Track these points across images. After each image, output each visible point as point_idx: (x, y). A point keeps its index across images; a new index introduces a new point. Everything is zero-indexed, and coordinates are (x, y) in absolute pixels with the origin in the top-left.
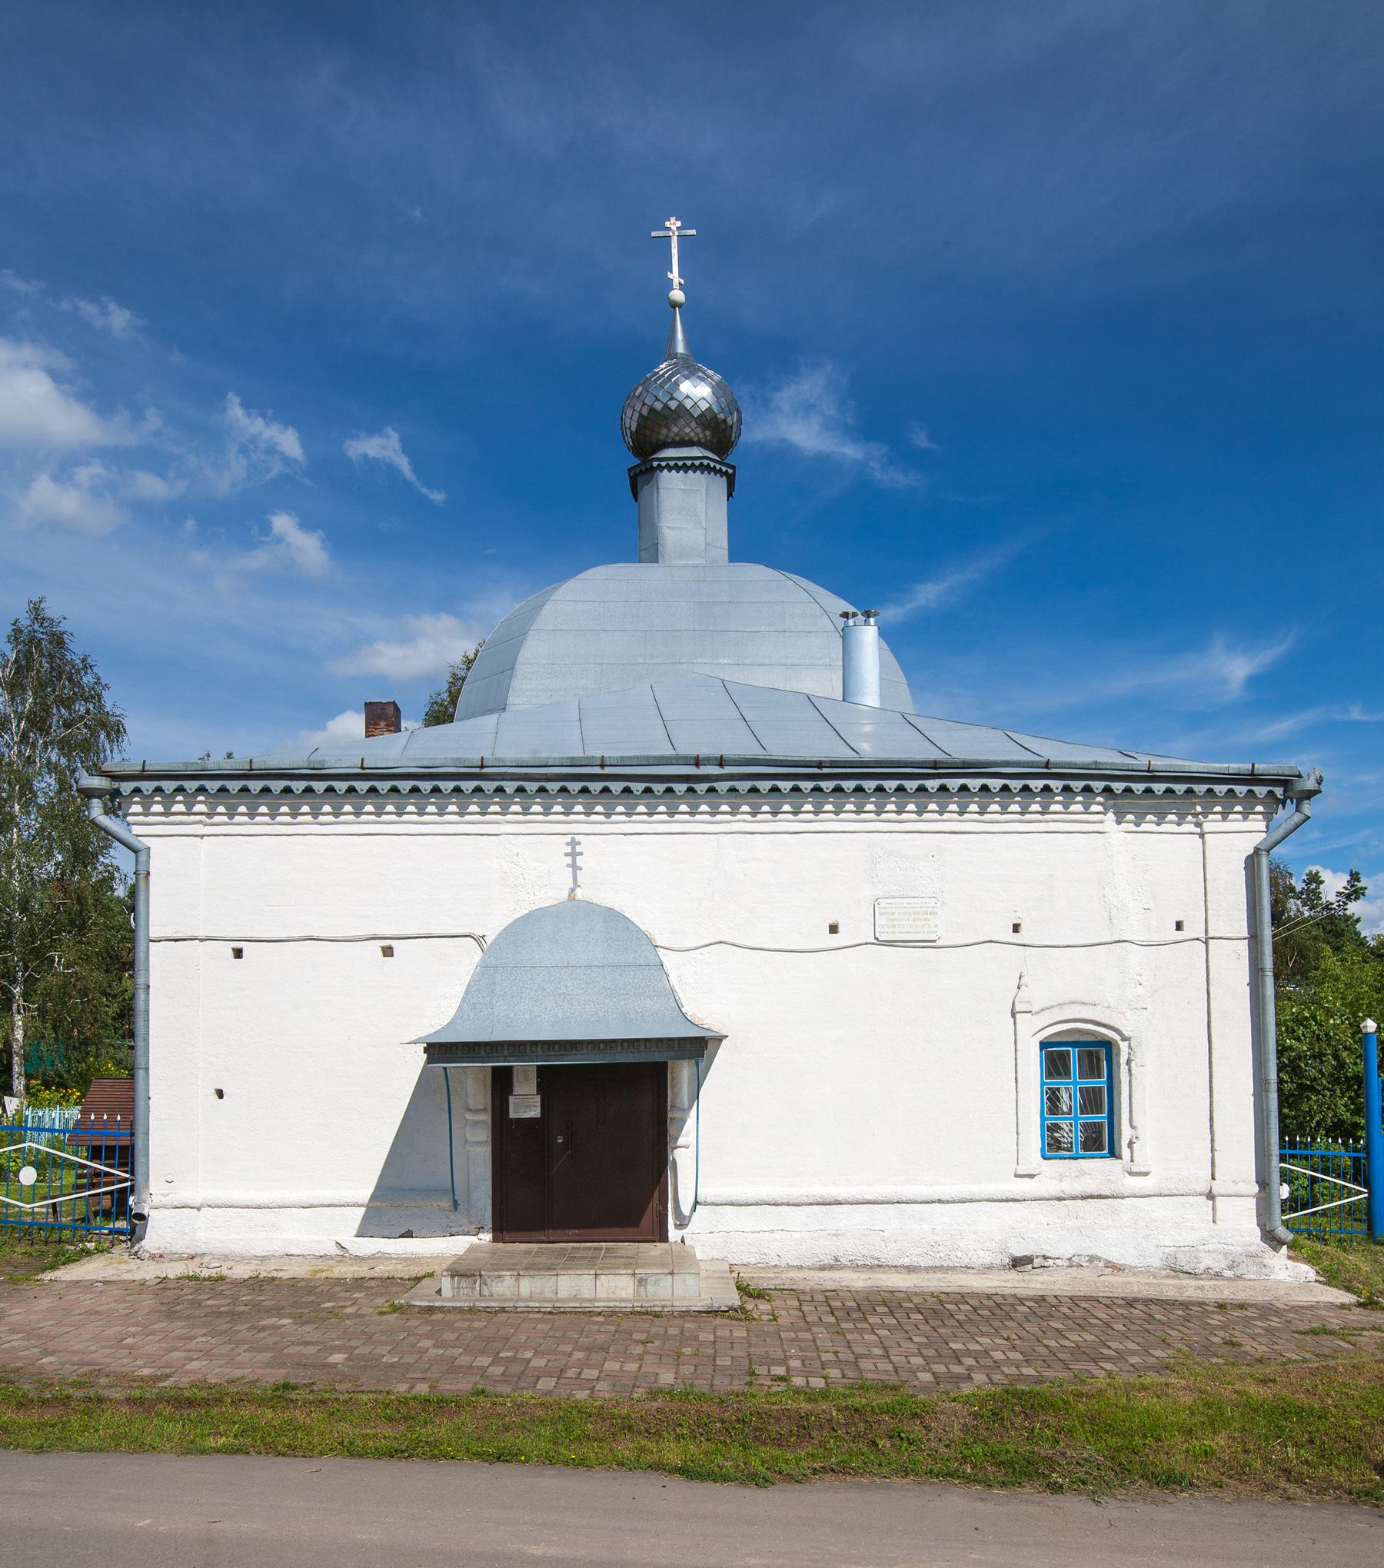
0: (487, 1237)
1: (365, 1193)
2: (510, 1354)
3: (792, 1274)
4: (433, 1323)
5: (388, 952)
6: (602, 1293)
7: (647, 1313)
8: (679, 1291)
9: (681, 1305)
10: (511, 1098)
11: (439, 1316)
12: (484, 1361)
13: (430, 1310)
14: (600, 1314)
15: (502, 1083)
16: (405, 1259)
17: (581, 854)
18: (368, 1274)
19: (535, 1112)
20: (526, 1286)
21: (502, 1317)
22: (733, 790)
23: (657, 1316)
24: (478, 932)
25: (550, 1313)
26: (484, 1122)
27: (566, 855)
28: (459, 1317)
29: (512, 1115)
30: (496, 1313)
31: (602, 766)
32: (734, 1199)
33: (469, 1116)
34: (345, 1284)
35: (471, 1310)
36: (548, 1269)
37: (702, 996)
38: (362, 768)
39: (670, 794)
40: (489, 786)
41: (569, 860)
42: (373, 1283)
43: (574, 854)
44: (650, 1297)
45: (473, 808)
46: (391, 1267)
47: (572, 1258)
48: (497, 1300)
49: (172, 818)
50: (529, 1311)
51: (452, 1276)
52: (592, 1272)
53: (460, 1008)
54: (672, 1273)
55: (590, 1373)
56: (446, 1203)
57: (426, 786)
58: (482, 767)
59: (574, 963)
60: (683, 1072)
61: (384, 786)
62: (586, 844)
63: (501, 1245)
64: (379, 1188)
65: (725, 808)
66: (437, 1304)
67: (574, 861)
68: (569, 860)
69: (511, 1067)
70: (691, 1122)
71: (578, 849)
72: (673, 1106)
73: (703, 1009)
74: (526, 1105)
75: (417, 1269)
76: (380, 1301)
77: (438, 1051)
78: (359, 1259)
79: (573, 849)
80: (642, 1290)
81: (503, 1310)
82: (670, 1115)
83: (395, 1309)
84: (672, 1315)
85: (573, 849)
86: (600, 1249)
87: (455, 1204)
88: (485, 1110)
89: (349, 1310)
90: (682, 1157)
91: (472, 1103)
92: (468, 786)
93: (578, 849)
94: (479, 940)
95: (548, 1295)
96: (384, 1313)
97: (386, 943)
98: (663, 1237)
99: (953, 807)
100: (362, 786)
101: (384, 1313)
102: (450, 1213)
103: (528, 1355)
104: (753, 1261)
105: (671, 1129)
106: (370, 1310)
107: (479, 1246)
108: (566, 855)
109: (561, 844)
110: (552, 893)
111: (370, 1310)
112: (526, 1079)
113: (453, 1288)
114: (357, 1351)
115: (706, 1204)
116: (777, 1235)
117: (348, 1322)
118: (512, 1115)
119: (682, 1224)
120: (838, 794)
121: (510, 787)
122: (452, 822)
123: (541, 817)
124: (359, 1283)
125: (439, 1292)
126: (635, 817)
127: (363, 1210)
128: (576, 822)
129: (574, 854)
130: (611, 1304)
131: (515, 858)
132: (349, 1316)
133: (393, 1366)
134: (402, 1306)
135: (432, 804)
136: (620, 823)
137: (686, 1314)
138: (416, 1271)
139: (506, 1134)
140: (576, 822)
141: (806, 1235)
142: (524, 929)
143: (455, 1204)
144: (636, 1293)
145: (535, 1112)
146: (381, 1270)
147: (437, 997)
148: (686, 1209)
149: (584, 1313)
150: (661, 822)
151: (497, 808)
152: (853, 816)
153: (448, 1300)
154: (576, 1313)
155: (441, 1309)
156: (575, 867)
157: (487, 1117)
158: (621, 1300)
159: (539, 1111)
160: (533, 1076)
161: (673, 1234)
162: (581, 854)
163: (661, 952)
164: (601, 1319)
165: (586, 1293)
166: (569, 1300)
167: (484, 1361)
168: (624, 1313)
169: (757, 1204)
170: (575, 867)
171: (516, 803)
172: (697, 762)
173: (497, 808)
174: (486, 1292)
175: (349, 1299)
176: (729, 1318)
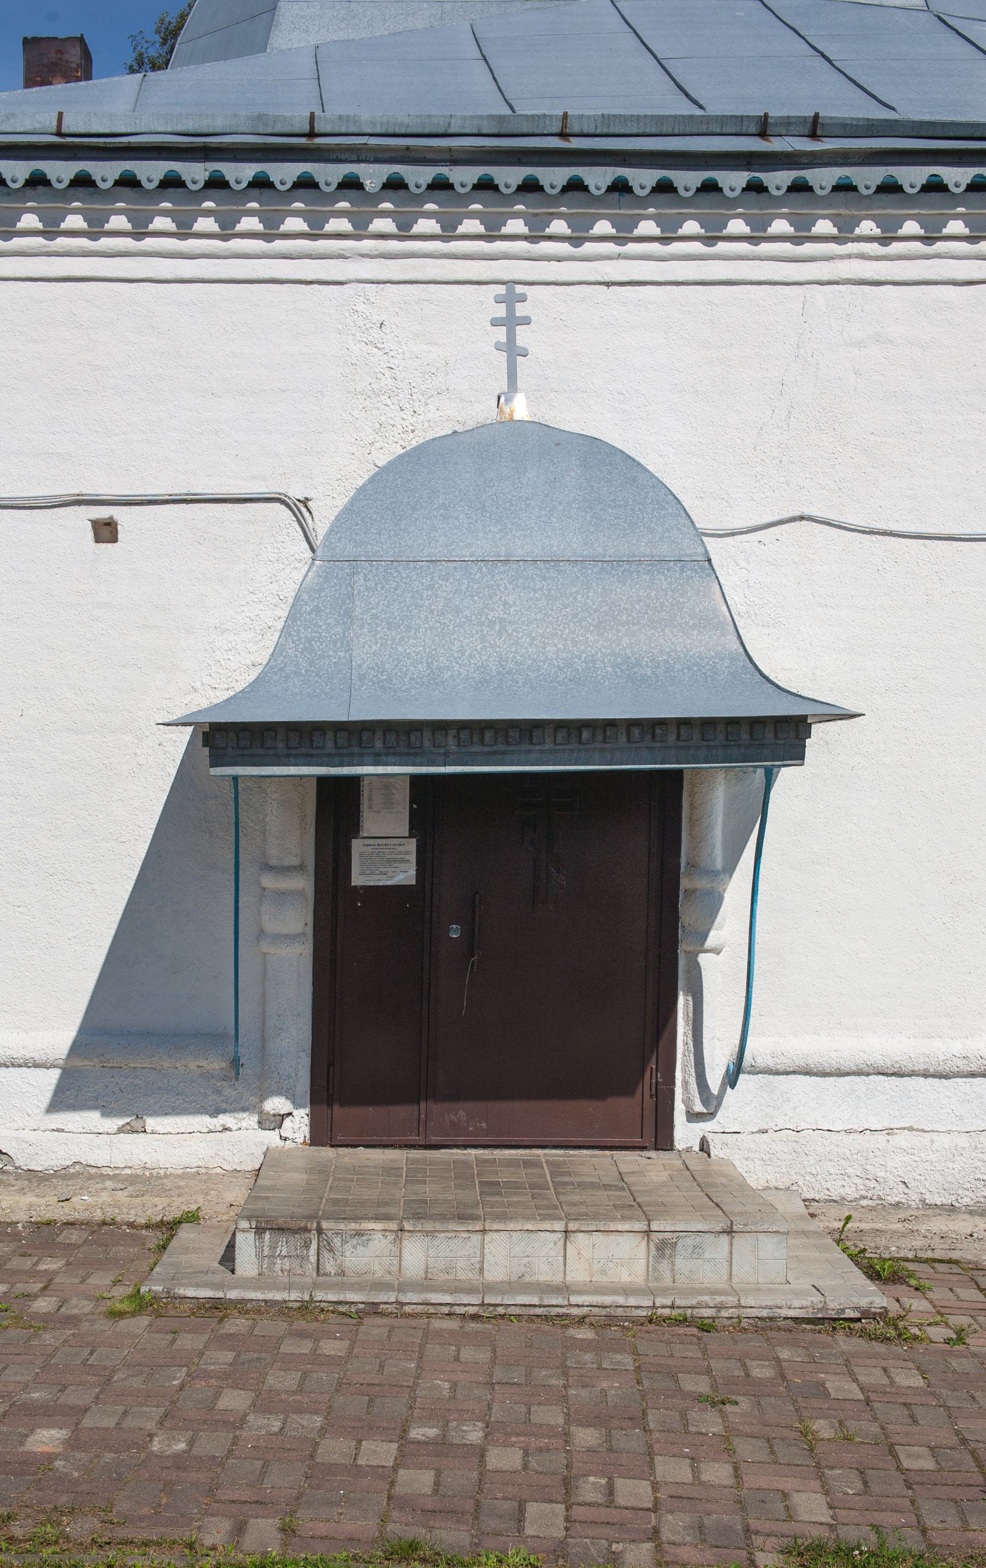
0: (299, 1125)
1: (59, 1038)
2: (433, 1432)
3: (939, 1224)
4: (227, 1341)
5: (106, 531)
6: (577, 1274)
7: (683, 1321)
8: (744, 1271)
9: (756, 1305)
10: (356, 844)
11: (236, 1325)
12: (379, 1452)
13: (218, 1308)
14: (581, 1320)
15: (338, 808)
16: (133, 1179)
17: (526, 321)
18: (61, 1213)
19: (404, 874)
20: (417, 1255)
21: (374, 1328)
22: (844, 187)
23: (706, 1327)
24: (296, 493)
25: (475, 1317)
26: (300, 893)
27: (495, 323)
28: (283, 1325)
29: (358, 879)
30: (361, 1315)
31: (563, 135)
32: (813, 1061)
33: (268, 881)
34: (16, 1236)
35: (305, 1308)
36: (462, 1218)
37: (788, 626)
38: (59, 134)
39: (713, 196)
40: (329, 174)
41: (501, 334)
42: (74, 1236)
43: (511, 322)
44: (682, 1282)
45: (294, 224)
46: (105, 1197)
47: (491, 1187)
48: (357, 1287)
49: (280, 245)
50: (430, 1312)
51: (259, 1231)
52: (559, 1226)
53: (279, 650)
54: (730, 1232)
55: (635, 1492)
56: (216, 1064)
57: (195, 172)
58: (312, 134)
59: (520, 553)
60: (716, 793)
61: (106, 172)
62: (536, 303)
63: (327, 1153)
64: (84, 1030)
65: (737, 226)
66: (233, 1294)
67: (511, 336)
68: (501, 334)
69: (355, 781)
70: (735, 892)
71: (521, 310)
72: (692, 865)
73: (795, 663)
74: (386, 858)
75: (161, 1202)
76: (101, 1280)
77: (223, 739)
78: (37, 1178)
79: (511, 310)
80: (664, 1266)
81: (373, 1309)
82: (685, 883)
83: (142, 1304)
84: (738, 1326)
85: (511, 310)
86: (535, 1164)
87: (236, 1063)
88: (301, 868)
89: (43, 1305)
90: (718, 969)
91: (274, 854)
92: (284, 173)
93: (521, 310)
94: (299, 508)
95: (464, 1274)
96: (121, 1315)
97: (103, 513)
98: (662, 1138)
99: (119, 222)
100: (61, 171)
101: (121, 1315)
102: (230, 1084)
103: (474, 1435)
104: (850, 1192)
105: (688, 915)
106: (87, 1306)
107: (282, 1151)
108: (495, 323)
109: (486, 303)
110: (464, 402)
111: (87, 1306)
112: (388, 803)
113: (260, 1256)
114: (87, 1422)
115: (755, 1071)
116: (902, 1140)
117: (48, 1338)
118: (358, 879)
119: (711, 1106)
120: (935, 196)
121: (373, 176)
122: (248, 255)
123: (83, 242)
124: (45, 1234)
125: (228, 1258)
126: (722, 247)
127: (55, 1074)
128: (549, 258)
129: (511, 322)
130: (607, 1300)
131: (375, 334)
132: (47, 1322)
133: (179, 1462)
134: (156, 1298)
135: (208, 213)
136: (603, 259)
137: (767, 1325)
138: (157, 1207)
139: (342, 914)
140: (549, 258)
141: (963, 1141)
142: (412, 481)
143: (236, 1063)
144: (653, 1272)
145: (404, 874)
146: (87, 1204)
147: (224, 628)
148: (714, 1080)
149: (546, 1318)
150: (687, 259)
151: (343, 225)
152: (917, 246)
153: (246, 1284)
154: (531, 1318)
155: (241, 1306)
156: (513, 351)
157: (304, 884)
158: (627, 1291)
159: (412, 871)
160: (402, 797)
161: (685, 1134)
162: (526, 321)
163: (710, 542)
164: (585, 1334)
165: (545, 1273)
166: (510, 1287)
167: (379, 1452)
168: (635, 1321)
169: (859, 1073)
170: (513, 351)
171: (384, 214)
172: (764, 128)
173: (343, 225)
174: (330, 1266)
175: (33, 1274)
176: (864, 1334)
